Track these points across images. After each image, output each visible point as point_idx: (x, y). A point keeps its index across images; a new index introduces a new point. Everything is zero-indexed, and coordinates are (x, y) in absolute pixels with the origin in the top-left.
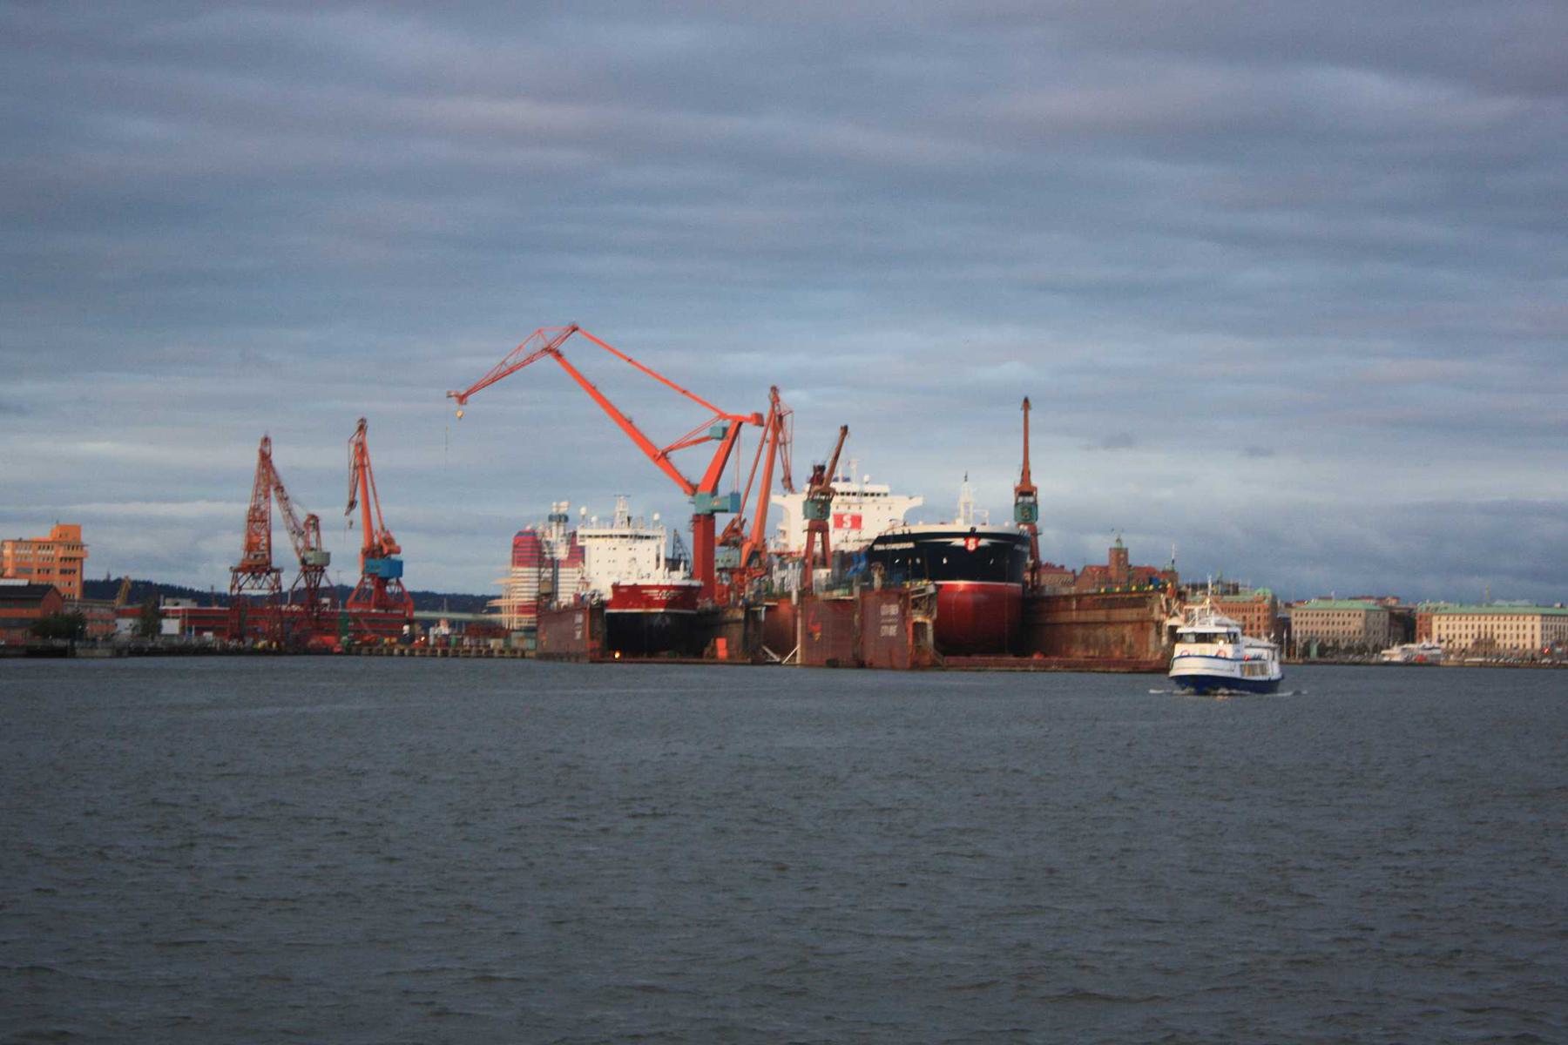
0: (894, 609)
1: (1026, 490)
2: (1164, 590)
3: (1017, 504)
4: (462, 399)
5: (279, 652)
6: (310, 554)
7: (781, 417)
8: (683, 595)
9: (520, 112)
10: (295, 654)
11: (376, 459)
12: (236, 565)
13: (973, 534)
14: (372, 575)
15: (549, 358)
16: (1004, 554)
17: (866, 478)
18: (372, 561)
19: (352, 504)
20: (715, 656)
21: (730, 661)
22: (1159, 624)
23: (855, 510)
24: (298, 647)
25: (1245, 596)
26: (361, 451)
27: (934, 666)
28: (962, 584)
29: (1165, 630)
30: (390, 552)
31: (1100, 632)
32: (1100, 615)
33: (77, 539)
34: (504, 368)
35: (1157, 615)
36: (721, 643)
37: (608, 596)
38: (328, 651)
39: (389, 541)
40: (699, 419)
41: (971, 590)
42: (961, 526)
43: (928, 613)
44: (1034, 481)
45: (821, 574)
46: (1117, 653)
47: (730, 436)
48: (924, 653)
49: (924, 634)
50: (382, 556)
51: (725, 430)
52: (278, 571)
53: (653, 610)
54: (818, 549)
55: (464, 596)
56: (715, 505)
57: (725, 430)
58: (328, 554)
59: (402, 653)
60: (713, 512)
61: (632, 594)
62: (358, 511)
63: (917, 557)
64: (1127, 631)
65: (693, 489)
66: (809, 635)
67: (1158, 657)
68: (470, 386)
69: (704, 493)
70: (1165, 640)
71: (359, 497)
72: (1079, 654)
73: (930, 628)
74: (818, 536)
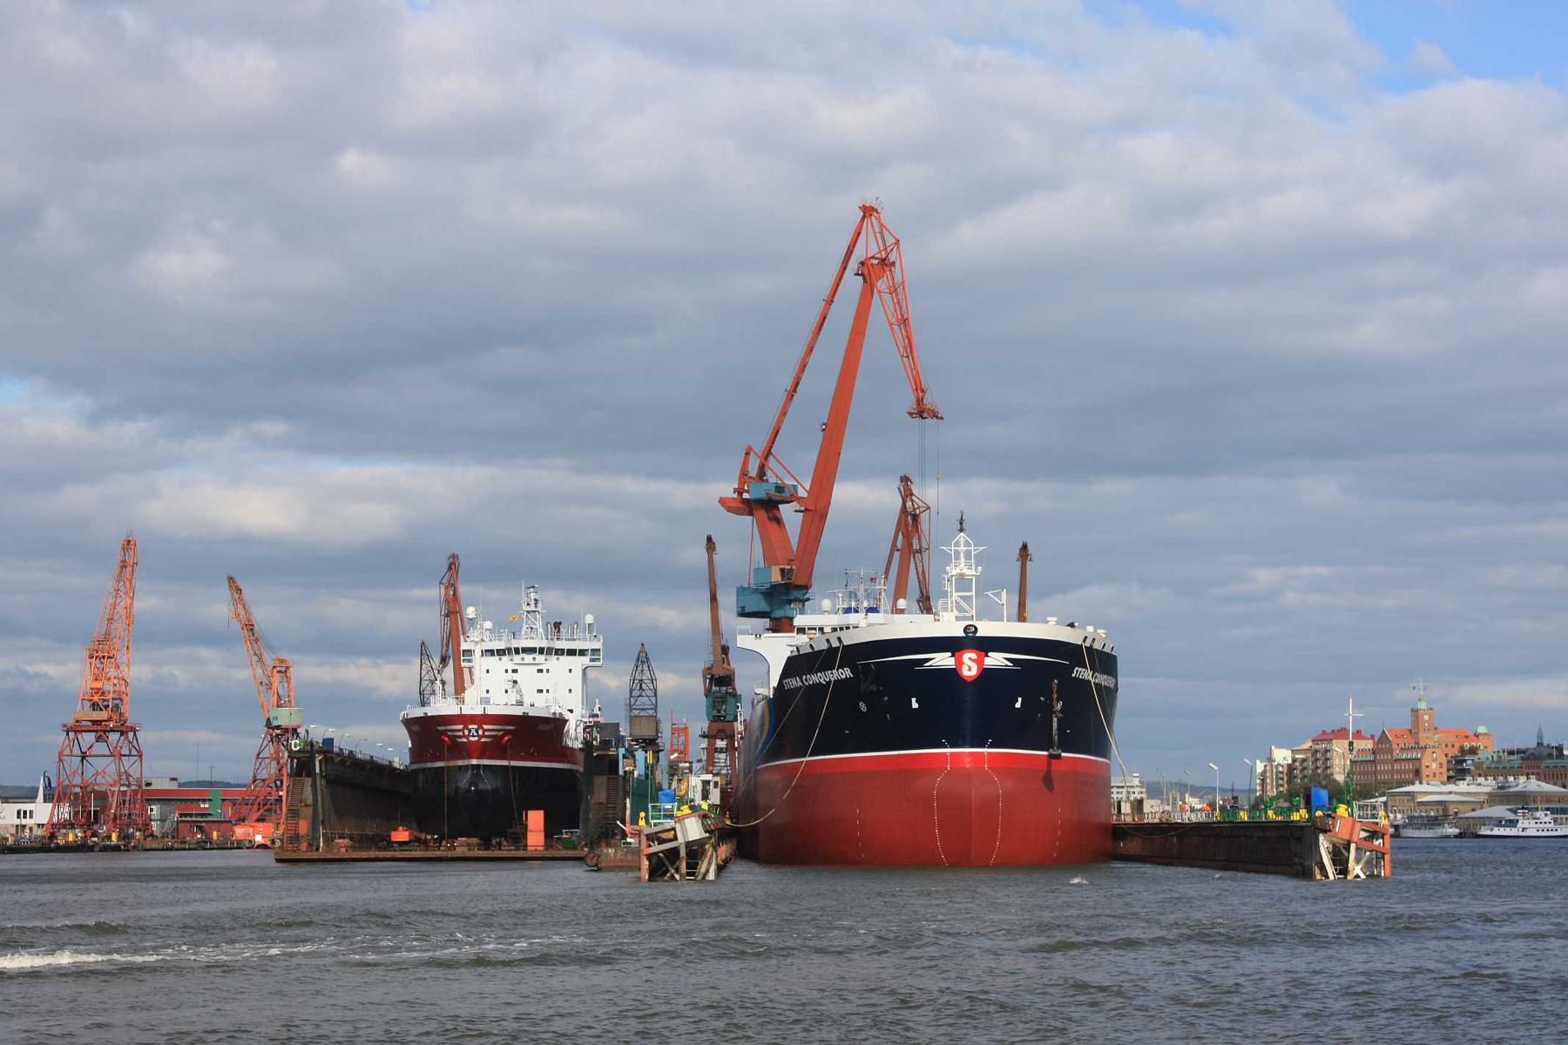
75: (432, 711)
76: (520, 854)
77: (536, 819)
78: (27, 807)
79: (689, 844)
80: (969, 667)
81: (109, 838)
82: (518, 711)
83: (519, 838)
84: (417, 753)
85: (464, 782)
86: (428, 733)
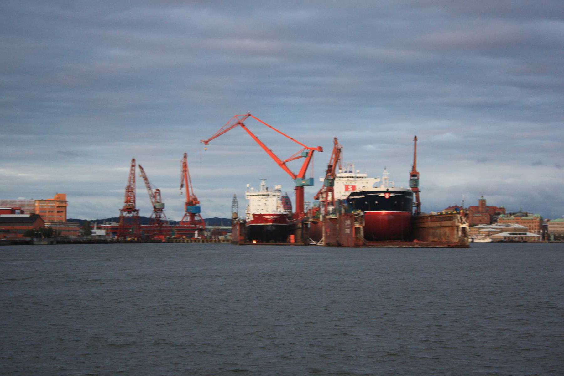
0: (348, 222)
1: (414, 175)
2: (459, 213)
3: (411, 180)
5: (138, 242)
6: (157, 204)
8: (280, 218)
9: (248, 43)
10: (146, 242)
11: (192, 171)
12: (121, 208)
13: (388, 192)
14: (189, 212)
15: (239, 127)
16: (401, 200)
17: (358, 171)
18: (189, 207)
19: (182, 186)
20: (290, 242)
21: (296, 244)
22: (458, 227)
23: (353, 184)
24: (148, 240)
25: (530, 217)
26: (185, 166)
27: (364, 245)
29: (460, 230)
30: (196, 203)
31: (438, 231)
32: (438, 224)
33: (64, 199)
34: (223, 131)
35: (457, 224)
36: (292, 237)
37: (252, 219)
38: (160, 242)
39: (195, 199)
40: (298, 149)
41: (387, 214)
42: (383, 188)
43: (361, 223)
44: (418, 169)
45: (331, 208)
46: (444, 239)
47: (309, 156)
48: (360, 240)
49: (360, 233)
50: (193, 205)
51: (307, 153)
52: (138, 211)
54: (330, 198)
56: (304, 183)
57: (307, 153)
58: (164, 204)
59: (188, 242)
60: (304, 185)
61: (259, 217)
62: (184, 189)
63: (366, 201)
64: (447, 230)
65: (295, 177)
66: (326, 233)
67: (457, 241)
68: (210, 137)
69: (299, 178)
70: (460, 234)
71: (184, 183)
72: (431, 239)
73: (362, 230)
74: (330, 194)
85: (269, 228)
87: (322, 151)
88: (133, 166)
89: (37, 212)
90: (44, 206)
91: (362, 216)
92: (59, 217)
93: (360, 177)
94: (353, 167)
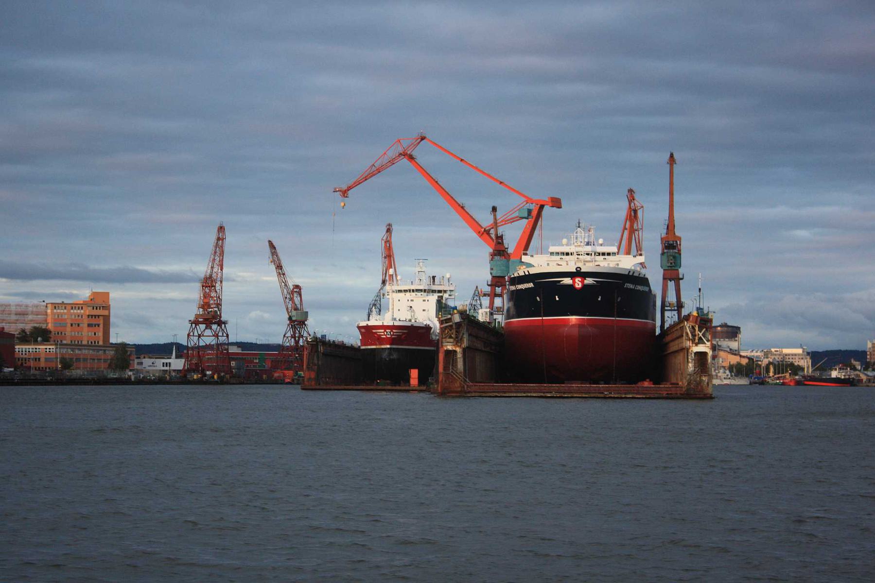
4: (345, 193)
6: (294, 313)
7: (635, 211)
13: (578, 273)
15: (405, 161)
16: (617, 293)
17: (601, 241)
27: (463, 394)
28: (573, 318)
34: (374, 169)
40: (510, 204)
41: (580, 325)
42: (570, 266)
43: (458, 341)
49: (455, 362)
53: (383, 347)
55: (827, 351)
57: (530, 211)
68: (351, 183)
70: (691, 367)
73: (459, 355)
75: (371, 323)
76: (407, 388)
77: (414, 373)
78: (168, 361)
79: (456, 323)
80: (578, 285)
81: (213, 377)
82: (409, 324)
83: (407, 380)
84: (363, 342)
85: (385, 355)
86: (367, 332)
87: (559, 207)
88: (219, 239)
89: (50, 326)
90: (62, 314)
91: (458, 325)
92: (91, 334)
93: (603, 254)
94: (592, 232)
